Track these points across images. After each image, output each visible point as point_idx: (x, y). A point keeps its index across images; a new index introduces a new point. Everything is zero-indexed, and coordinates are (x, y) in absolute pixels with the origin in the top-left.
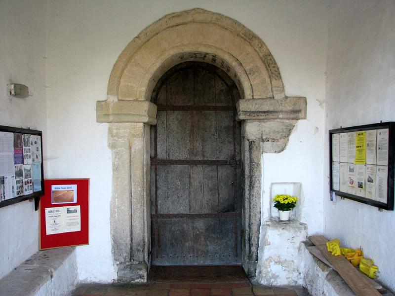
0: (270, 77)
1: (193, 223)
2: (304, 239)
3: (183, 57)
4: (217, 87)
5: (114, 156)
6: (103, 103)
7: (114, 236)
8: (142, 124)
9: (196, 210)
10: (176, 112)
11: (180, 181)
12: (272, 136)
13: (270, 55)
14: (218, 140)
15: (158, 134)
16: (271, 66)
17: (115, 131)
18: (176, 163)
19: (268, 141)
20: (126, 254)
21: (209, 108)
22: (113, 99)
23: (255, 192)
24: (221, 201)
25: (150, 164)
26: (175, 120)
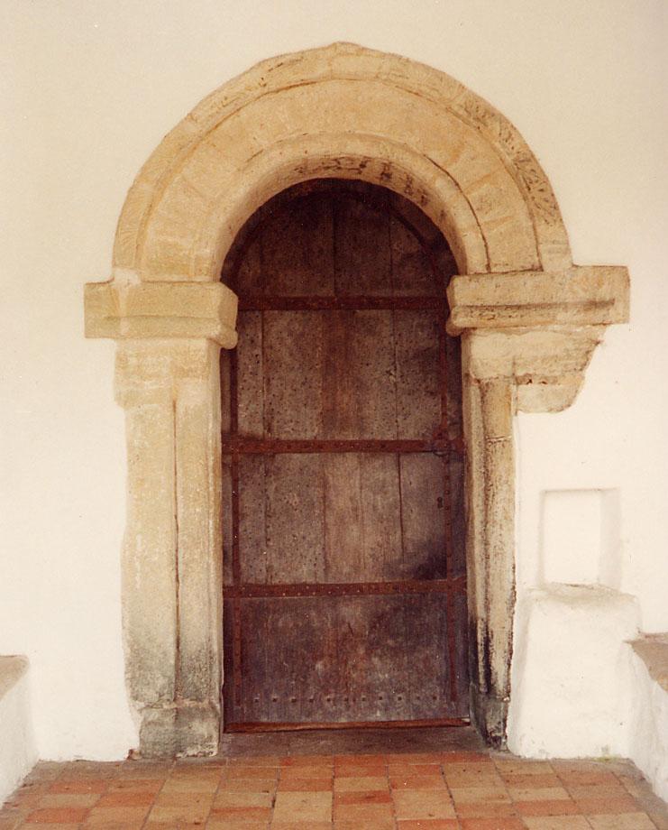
0: (531, 215)
1: (334, 607)
2: (633, 636)
3: (306, 167)
4: (395, 247)
5: (133, 425)
6: (102, 289)
7: (131, 632)
8: (205, 340)
9: (344, 573)
10: (289, 315)
11: (299, 495)
12: (539, 370)
13: (530, 158)
14: (399, 385)
15: (239, 373)
16: (535, 187)
17: (133, 361)
18: (289, 447)
19: (531, 381)
20: (161, 680)
21: (373, 304)
22: (128, 278)
23: (498, 507)
24: (410, 548)
25: (220, 452)
26: (285, 335)
